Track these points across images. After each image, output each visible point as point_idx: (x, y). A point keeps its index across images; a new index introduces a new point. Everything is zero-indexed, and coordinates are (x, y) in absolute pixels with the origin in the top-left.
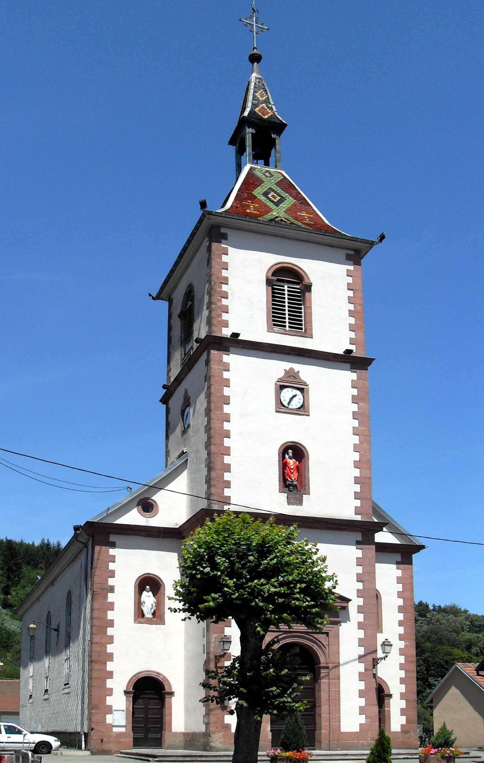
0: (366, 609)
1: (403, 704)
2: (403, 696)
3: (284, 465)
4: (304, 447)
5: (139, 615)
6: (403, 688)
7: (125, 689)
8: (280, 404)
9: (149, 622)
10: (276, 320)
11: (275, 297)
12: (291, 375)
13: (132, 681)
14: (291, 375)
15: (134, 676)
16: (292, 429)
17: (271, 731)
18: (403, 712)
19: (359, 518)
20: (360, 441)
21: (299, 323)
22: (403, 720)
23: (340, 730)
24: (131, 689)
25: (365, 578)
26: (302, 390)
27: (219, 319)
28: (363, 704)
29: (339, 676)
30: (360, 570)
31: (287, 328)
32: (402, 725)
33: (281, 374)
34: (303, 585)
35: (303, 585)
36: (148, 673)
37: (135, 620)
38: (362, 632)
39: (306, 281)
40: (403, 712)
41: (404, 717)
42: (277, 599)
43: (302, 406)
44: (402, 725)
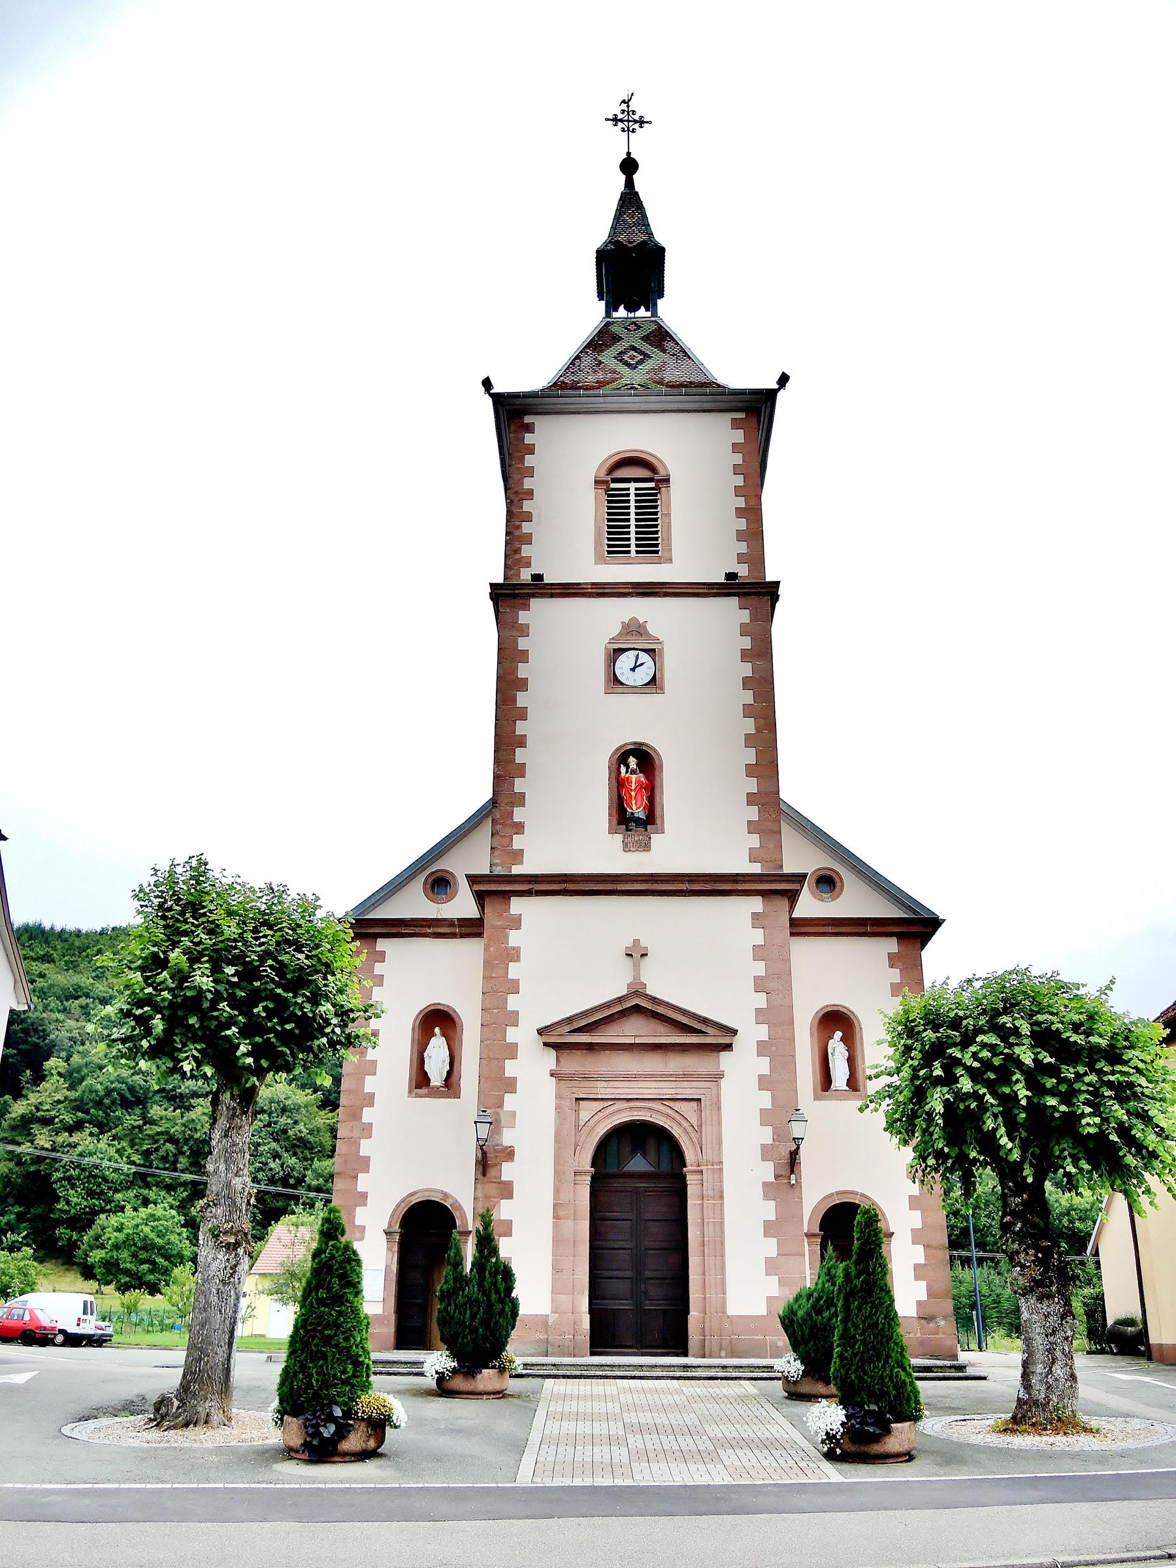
0: (774, 1049)
1: (918, 1254)
2: (917, 1237)
3: (619, 785)
4: (655, 751)
5: (421, 1080)
6: (915, 1219)
7: (386, 1227)
8: (614, 682)
9: (435, 1093)
10: (615, 545)
11: (616, 504)
12: (634, 629)
13: (400, 1210)
14: (634, 629)
15: (403, 1200)
16: (633, 720)
17: (591, 1311)
18: (919, 1272)
19: (756, 868)
20: (756, 729)
21: (650, 545)
22: (920, 1291)
23: (724, 1312)
24: (397, 1228)
25: (772, 985)
26: (650, 652)
27: (517, 556)
28: (774, 1253)
29: (722, 1192)
30: (760, 968)
31: (633, 554)
32: (919, 1303)
33: (616, 630)
34: (206, 1005)
35: (206, 1005)
36: (427, 1194)
37: (410, 1092)
38: (767, 1094)
39: (662, 473)
40: (919, 1272)
41: (922, 1285)
42: (134, 1029)
43: (617, 681)
44: (919, 1303)
